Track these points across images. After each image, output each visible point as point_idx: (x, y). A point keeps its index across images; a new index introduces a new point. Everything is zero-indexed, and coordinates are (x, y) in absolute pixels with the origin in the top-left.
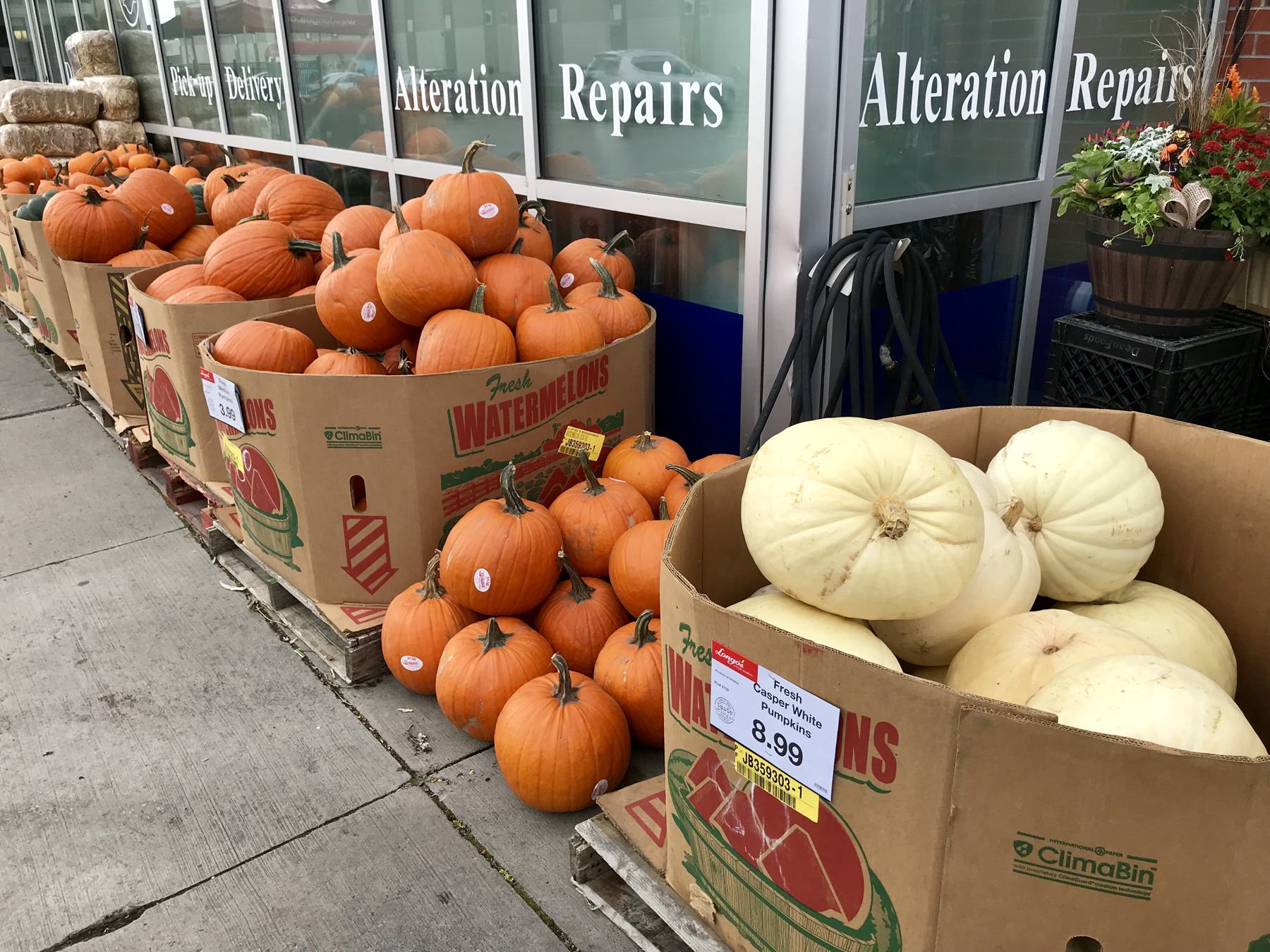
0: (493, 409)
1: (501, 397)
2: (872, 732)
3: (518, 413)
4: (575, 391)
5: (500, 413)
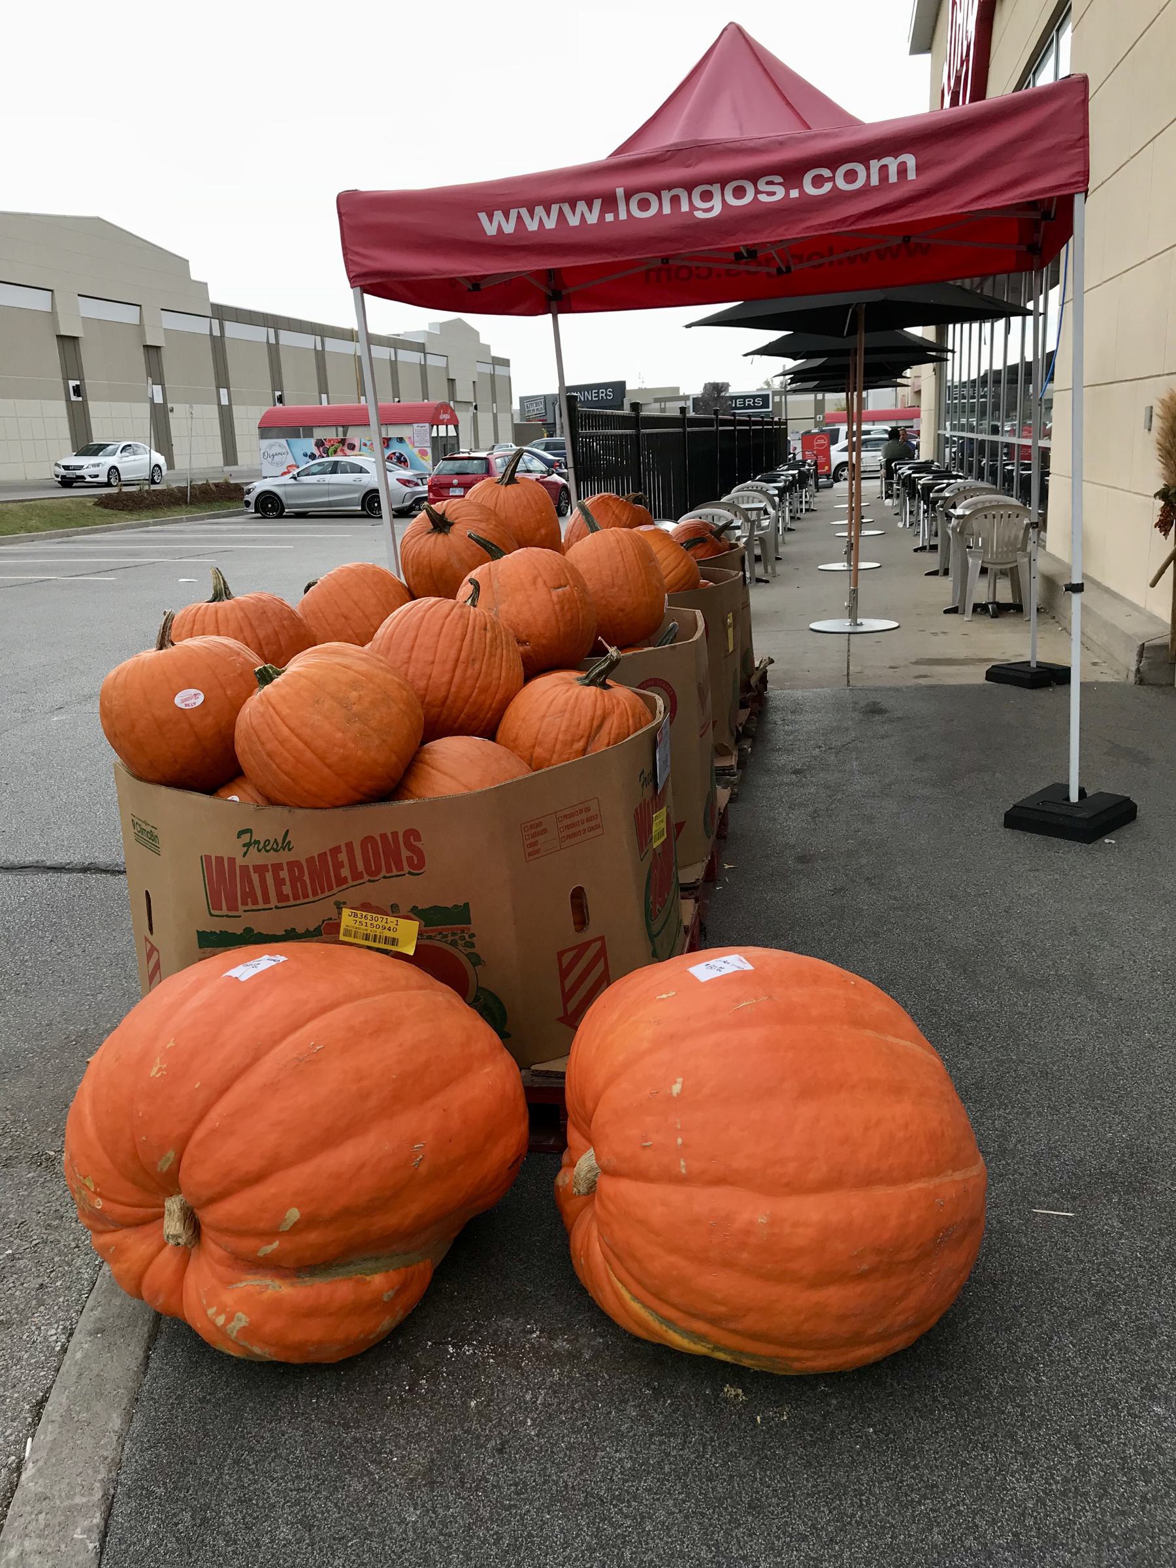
0: (244, 868)
1: (255, 858)
2: (401, 839)
3: (279, 883)
4: (360, 866)
5: (255, 877)
